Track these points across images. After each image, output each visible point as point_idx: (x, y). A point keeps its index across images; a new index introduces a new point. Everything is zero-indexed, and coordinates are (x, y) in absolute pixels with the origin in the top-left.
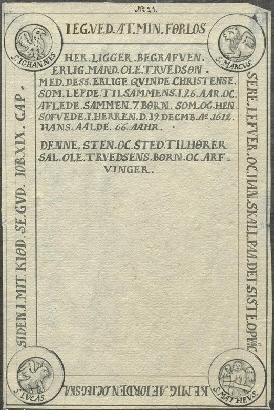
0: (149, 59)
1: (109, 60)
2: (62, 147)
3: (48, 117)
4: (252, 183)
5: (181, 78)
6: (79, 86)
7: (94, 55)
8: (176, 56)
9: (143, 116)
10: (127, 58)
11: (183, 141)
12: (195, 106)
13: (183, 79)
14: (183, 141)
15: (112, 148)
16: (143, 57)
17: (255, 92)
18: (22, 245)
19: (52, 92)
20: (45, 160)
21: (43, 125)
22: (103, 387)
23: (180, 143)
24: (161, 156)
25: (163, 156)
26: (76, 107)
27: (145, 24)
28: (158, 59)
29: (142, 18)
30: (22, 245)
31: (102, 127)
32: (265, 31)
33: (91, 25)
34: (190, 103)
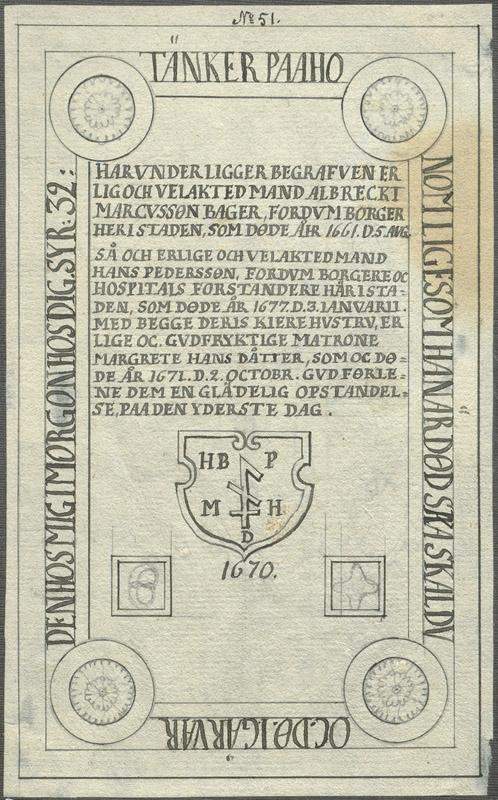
3: (361, 213)
4: (267, 193)
12: (105, 360)
13: (100, 227)
28: (303, 175)
29: (256, 40)
30: (271, 231)
34: (160, 303)
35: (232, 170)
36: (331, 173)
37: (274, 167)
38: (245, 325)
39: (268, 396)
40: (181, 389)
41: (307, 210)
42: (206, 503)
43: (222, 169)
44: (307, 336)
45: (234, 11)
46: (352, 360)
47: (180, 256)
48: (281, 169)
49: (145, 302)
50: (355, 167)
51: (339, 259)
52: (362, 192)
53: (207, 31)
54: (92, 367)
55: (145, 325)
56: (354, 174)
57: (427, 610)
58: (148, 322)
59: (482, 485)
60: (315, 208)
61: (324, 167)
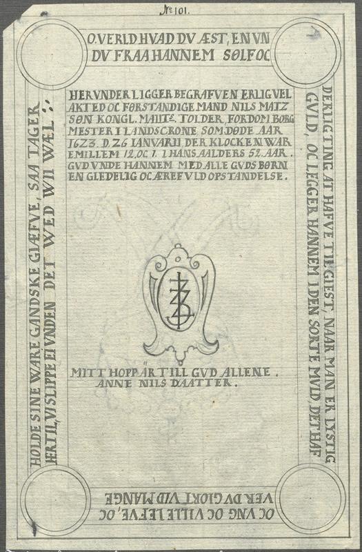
0: (185, 96)
2: (180, 58)
8: (211, 92)
10: (217, 119)
11: (233, 369)
14: (233, 369)
18: (242, 132)
20: (36, 183)
21: (126, 163)
22: (265, 51)
23: (231, 370)
27: (80, 369)
30: (242, 132)
31: (50, 321)
32: (342, 63)
35: (150, 93)
36: (328, 216)
38: (242, 155)
41: (97, 54)
43: (332, 455)
44: (204, 103)
45: (160, 7)
48: (180, 92)
49: (206, 127)
50: (225, 91)
52: (252, 54)
53: (148, 18)
60: (188, 34)
61: (334, 375)
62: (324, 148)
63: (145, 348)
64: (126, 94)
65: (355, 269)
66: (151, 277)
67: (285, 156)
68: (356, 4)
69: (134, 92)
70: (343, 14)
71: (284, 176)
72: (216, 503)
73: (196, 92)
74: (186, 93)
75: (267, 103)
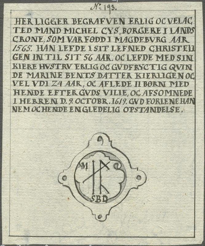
0: (82, 22)
1: (50, 23)
4: (185, 102)
5: (157, 46)
6: (56, 63)
7: (36, 19)
9: (29, 30)
15: (78, 73)
16: (77, 20)
17: (75, 19)
19: (81, 110)
24: (149, 83)
25: (150, 83)
26: (21, 76)
33: (168, 19)
37: (151, 28)
39: (117, 95)
40: (76, 73)
42: (76, 69)
45: (92, 5)
46: (128, 108)
47: (159, 76)
51: (25, 110)
54: (194, 72)
55: (70, 76)
56: (114, 22)
57: (93, 32)
58: (70, 74)
59: (118, 152)
62: (34, 59)
63: (147, 65)
64: (129, 76)
65: (203, 145)
66: (101, 185)
67: (82, 42)
68: (203, 2)
69: (36, 19)
70: (195, 10)
71: (180, 110)
72: (79, 29)
73: (90, 21)
74: (82, 21)
75: (162, 55)
